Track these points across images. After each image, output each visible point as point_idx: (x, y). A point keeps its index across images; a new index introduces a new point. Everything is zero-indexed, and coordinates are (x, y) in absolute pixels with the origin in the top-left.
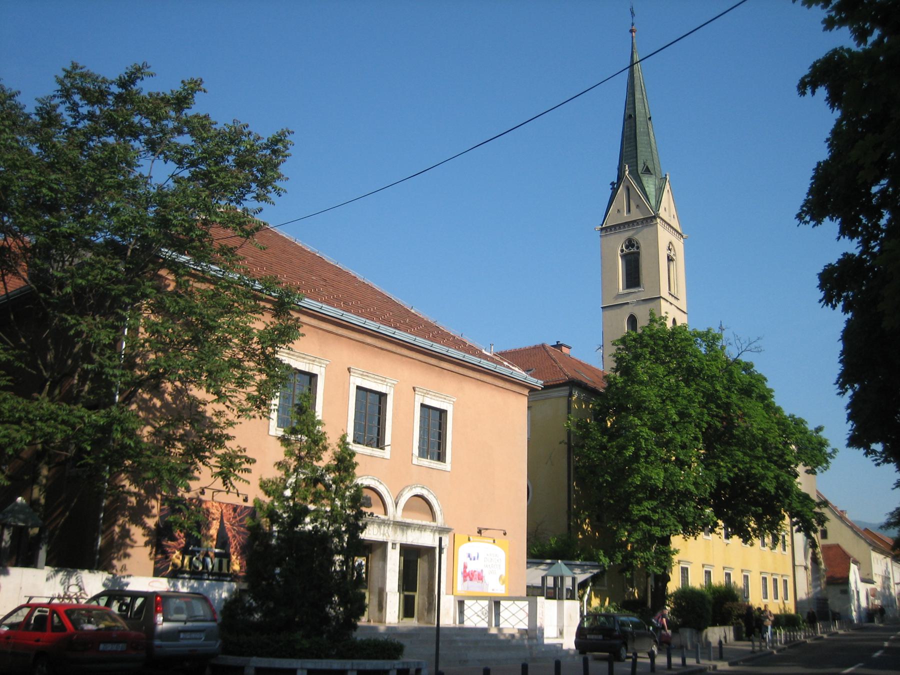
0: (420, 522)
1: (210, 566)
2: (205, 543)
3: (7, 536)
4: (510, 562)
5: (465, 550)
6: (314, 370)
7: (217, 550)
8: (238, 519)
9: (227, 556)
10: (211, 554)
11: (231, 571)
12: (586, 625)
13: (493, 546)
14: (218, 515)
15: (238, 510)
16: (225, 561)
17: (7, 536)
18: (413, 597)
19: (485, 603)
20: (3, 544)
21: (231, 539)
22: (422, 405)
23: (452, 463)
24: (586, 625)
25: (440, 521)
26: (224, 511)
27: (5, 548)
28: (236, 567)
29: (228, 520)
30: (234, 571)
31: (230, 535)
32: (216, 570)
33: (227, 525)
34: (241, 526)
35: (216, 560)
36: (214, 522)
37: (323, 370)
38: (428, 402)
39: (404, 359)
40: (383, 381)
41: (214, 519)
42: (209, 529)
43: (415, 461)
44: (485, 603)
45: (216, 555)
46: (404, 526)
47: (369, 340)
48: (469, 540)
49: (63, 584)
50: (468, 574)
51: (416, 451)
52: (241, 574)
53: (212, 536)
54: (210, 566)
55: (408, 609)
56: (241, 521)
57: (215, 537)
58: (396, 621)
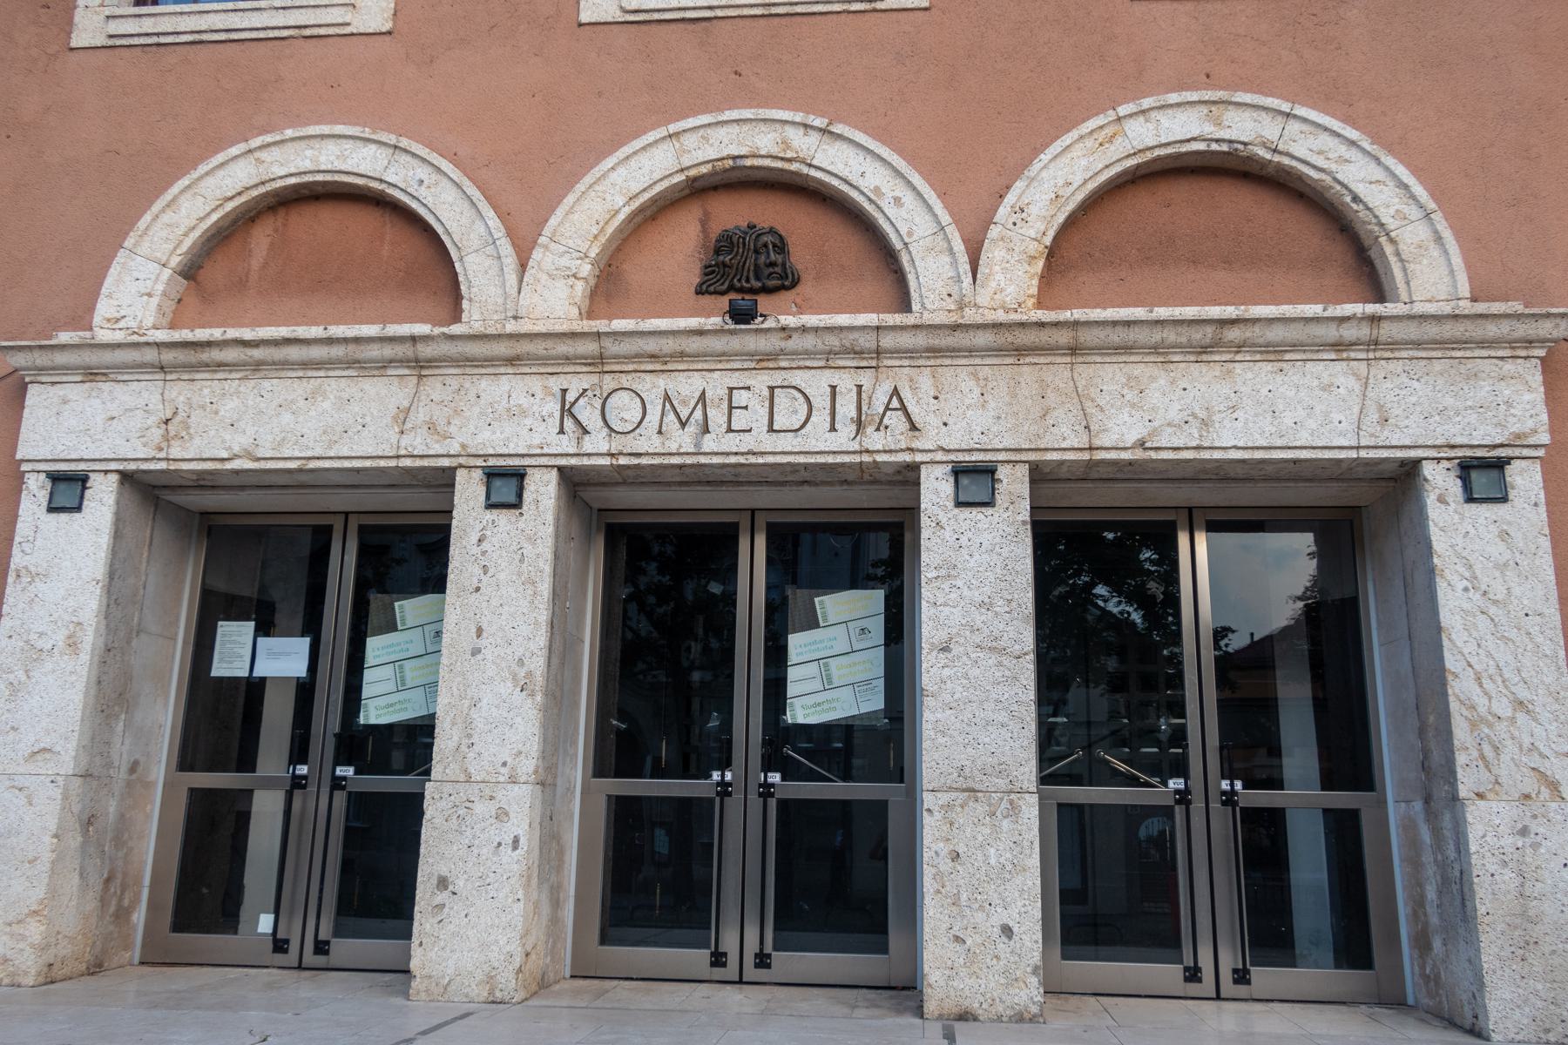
38: (235, 755)
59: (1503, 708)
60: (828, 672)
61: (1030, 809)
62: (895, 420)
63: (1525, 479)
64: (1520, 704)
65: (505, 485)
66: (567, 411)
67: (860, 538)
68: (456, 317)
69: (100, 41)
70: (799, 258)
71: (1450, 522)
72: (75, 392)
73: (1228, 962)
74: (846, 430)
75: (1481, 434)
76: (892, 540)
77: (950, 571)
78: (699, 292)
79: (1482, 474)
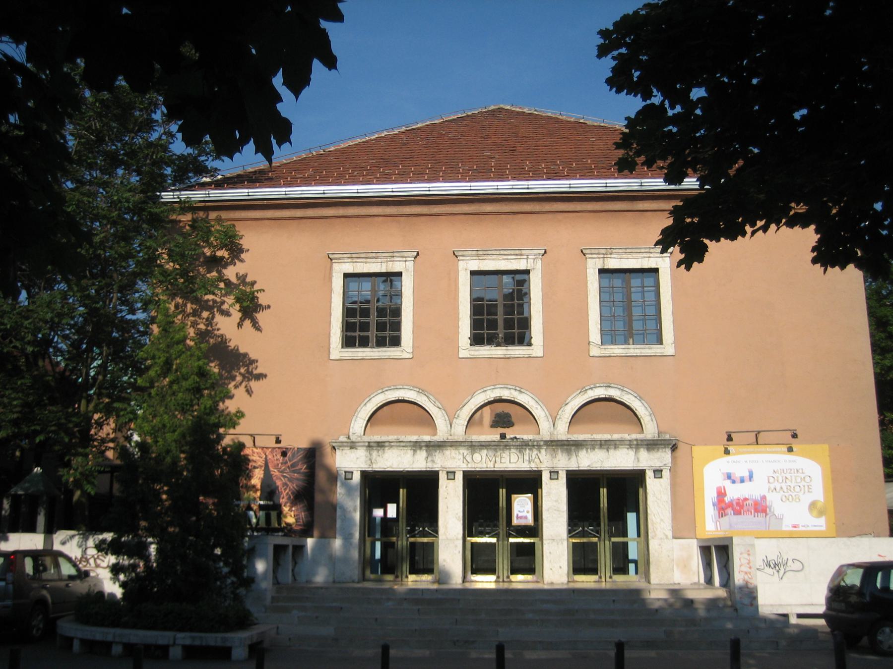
0: (607, 437)
1: (254, 520)
2: (246, 495)
3: (6, 504)
4: (837, 480)
5: (714, 472)
6: (396, 267)
7: (262, 502)
8: (289, 464)
9: (278, 508)
10: (255, 508)
11: (283, 525)
12: (802, 209)
13: (789, 457)
14: (260, 462)
15: (289, 454)
16: (274, 514)
17: (6, 504)
18: (625, 545)
19: (530, 521)
20: (3, 512)
21: (281, 488)
22: (602, 271)
23: (676, 342)
24: (802, 209)
25: (650, 430)
26: (270, 457)
27: (5, 516)
28: (290, 520)
29: (276, 466)
30: (288, 524)
31: (279, 483)
32: (262, 524)
33: (275, 472)
34: (294, 472)
35: (261, 514)
36: (257, 471)
37: (410, 264)
38: (613, 263)
39: (560, 216)
40: (519, 254)
41: (255, 468)
42: (249, 477)
43: (595, 351)
44: (530, 521)
45: (261, 507)
46: (570, 446)
47: (488, 208)
48: (727, 452)
49: (80, 546)
50: (730, 505)
51: (595, 335)
52: (298, 528)
53: (254, 486)
54: (254, 520)
55: (583, 561)
56: (293, 466)
57: (259, 486)
58: (565, 579)
59: (658, 521)
60: (522, 507)
61: (565, 543)
62: (537, 460)
63: (666, 473)
64: (661, 520)
65: (451, 474)
66: (464, 458)
67: (530, 483)
68: (435, 434)
69: (338, 358)
70: (513, 419)
71: (650, 481)
72: (347, 451)
73: (608, 575)
74: (526, 463)
75: (657, 464)
76: (261, 172)
77: (549, 494)
78: (492, 426)
79: (658, 473)
